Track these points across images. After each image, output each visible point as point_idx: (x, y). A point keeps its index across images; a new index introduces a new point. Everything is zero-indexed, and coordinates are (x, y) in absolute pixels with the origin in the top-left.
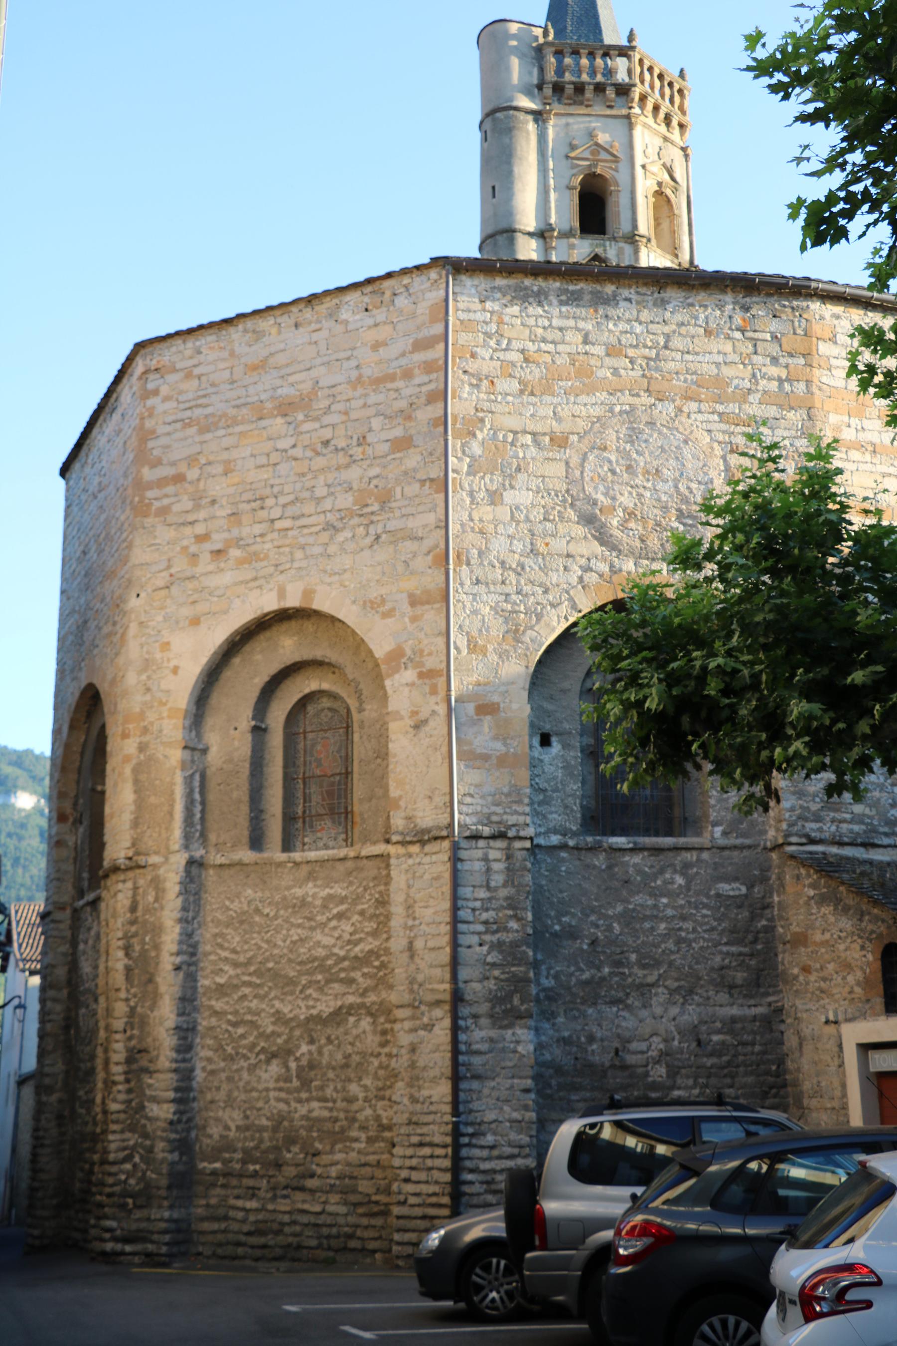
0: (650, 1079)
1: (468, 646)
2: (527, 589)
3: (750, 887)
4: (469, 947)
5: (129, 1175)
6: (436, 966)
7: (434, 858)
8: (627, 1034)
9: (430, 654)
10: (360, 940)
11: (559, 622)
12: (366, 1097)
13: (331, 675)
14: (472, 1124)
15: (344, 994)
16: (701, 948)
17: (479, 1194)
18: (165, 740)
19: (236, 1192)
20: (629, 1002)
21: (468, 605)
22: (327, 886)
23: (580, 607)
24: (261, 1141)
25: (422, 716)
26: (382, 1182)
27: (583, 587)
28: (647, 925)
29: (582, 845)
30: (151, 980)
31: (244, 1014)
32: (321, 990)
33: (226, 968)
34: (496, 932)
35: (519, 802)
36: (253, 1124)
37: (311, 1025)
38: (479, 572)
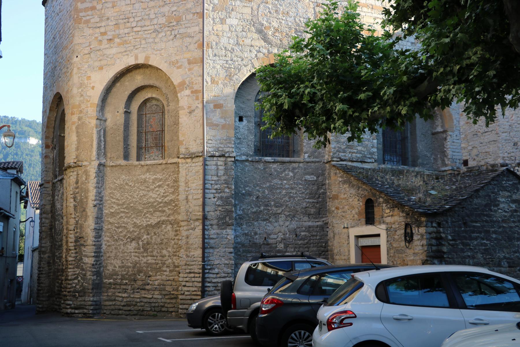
0: (278, 249)
2: (235, 59)
3: (318, 177)
4: (210, 198)
5: (76, 284)
6: (197, 206)
8: (270, 232)
11: (247, 72)
12: (169, 255)
14: (210, 265)
15: (161, 216)
17: (212, 291)
20: (271, 220)
21: (211, 64)
27: (257, 59)
28: (278, 191)
29: (254, 160)
33: (114, 206)
34: (220, 193)
35: (230, 143)
37: (148, 228)
38: (216, 51)
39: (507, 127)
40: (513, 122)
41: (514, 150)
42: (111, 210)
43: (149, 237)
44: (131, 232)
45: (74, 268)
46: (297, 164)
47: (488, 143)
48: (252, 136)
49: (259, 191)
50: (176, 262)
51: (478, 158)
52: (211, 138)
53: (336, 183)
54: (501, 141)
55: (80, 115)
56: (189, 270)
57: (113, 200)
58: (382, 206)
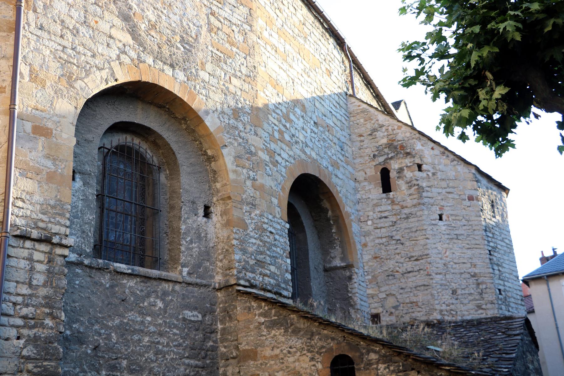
1: (30, 75)
2: (80, 49)
3: (204, 316)
4: (7, 339)
11: (101, 82)
16: (172, 359)
21: (33, 42)
23: (117, 76)
27: (120, 63)
28: (136, 337)
29: (94, 264)
35: (62, 215)
38: (42, 20)
39: (441, 266)
40: (448, 259)
41: (454, 301)
46: (171, 285)
47: (414, 289)
48: (91, 215)
49: (100, 334)
51: (397, 312)
52: (23, 197)
53: (252, 327)
54: (436, 286)
58: (377, 369)
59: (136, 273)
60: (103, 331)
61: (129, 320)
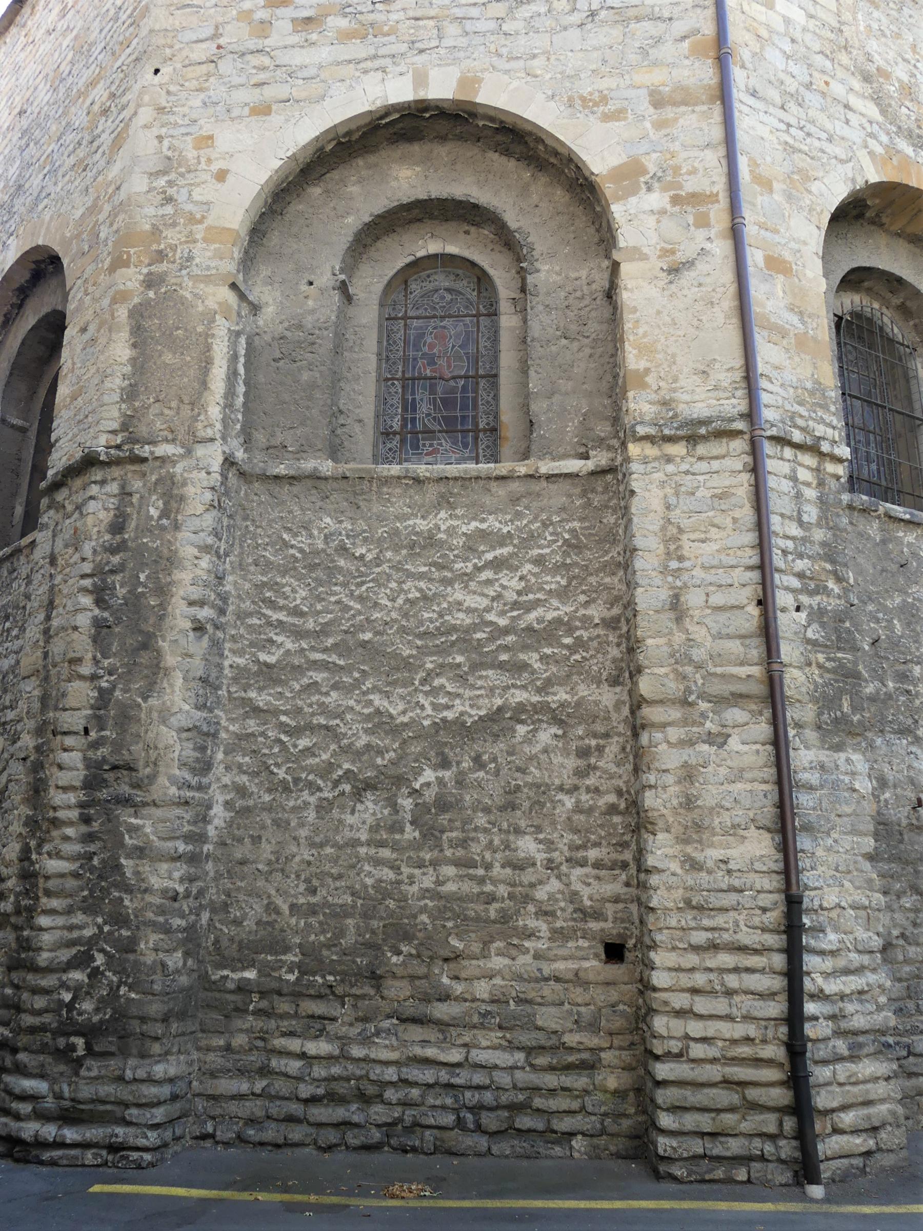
5: (78, 992)
6: (729, 637)
7: (715, 464)
9: (690, 173)
10: (537, 603)
12: (550, 861)
13: (462, 236)
15: (508, 687)
17: (826, 1039)
18: (196, 271)
19: (285, 1024)
22: (474, 519)
24: (341, 933)
25: (680, 257)
26: (583, 1009)
30: (147, 643)
31: (313, 714)
32: (462, 679)
33: (279, 639)
36: (326, 904)
37: (443, 737)
42: (263, 657)
43: (447, 774)
44: (359, 754)
45: (69, 911)
50: (585, 892)
55: (153, 268)
56: (709, 935)
57: (275, 616)
59: (916, 520)
60: (881, 615)
61: (914, 599)
